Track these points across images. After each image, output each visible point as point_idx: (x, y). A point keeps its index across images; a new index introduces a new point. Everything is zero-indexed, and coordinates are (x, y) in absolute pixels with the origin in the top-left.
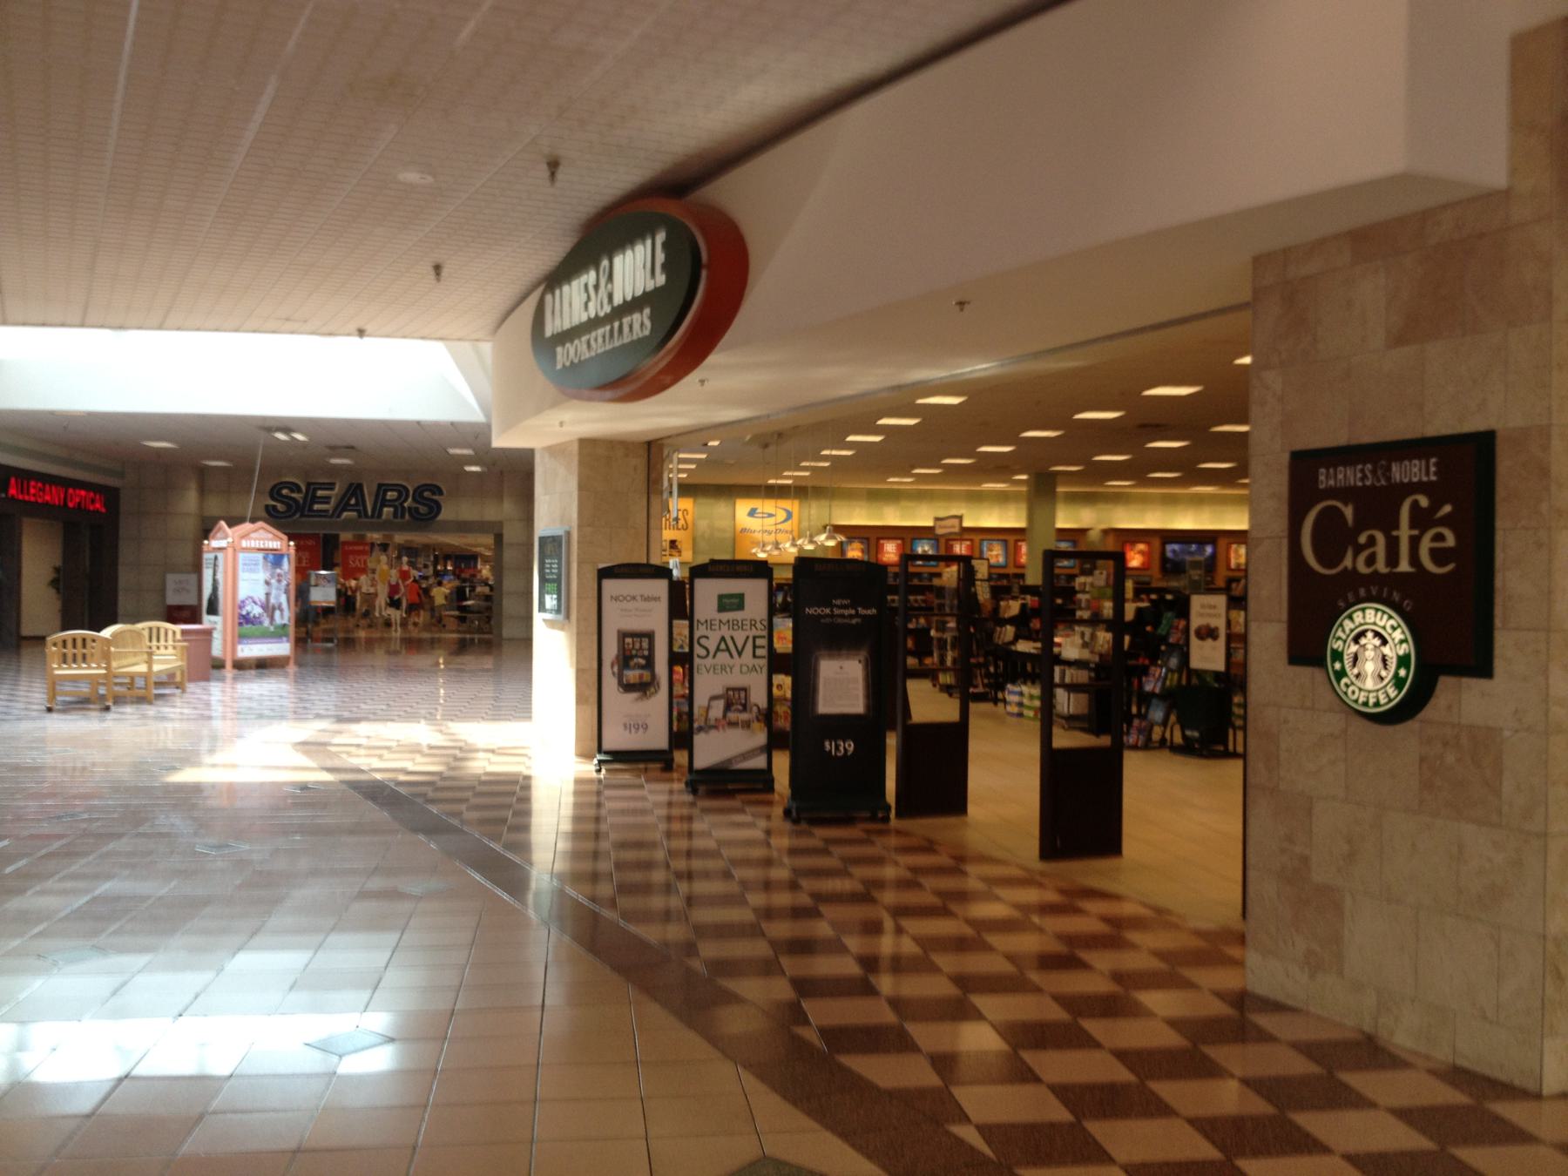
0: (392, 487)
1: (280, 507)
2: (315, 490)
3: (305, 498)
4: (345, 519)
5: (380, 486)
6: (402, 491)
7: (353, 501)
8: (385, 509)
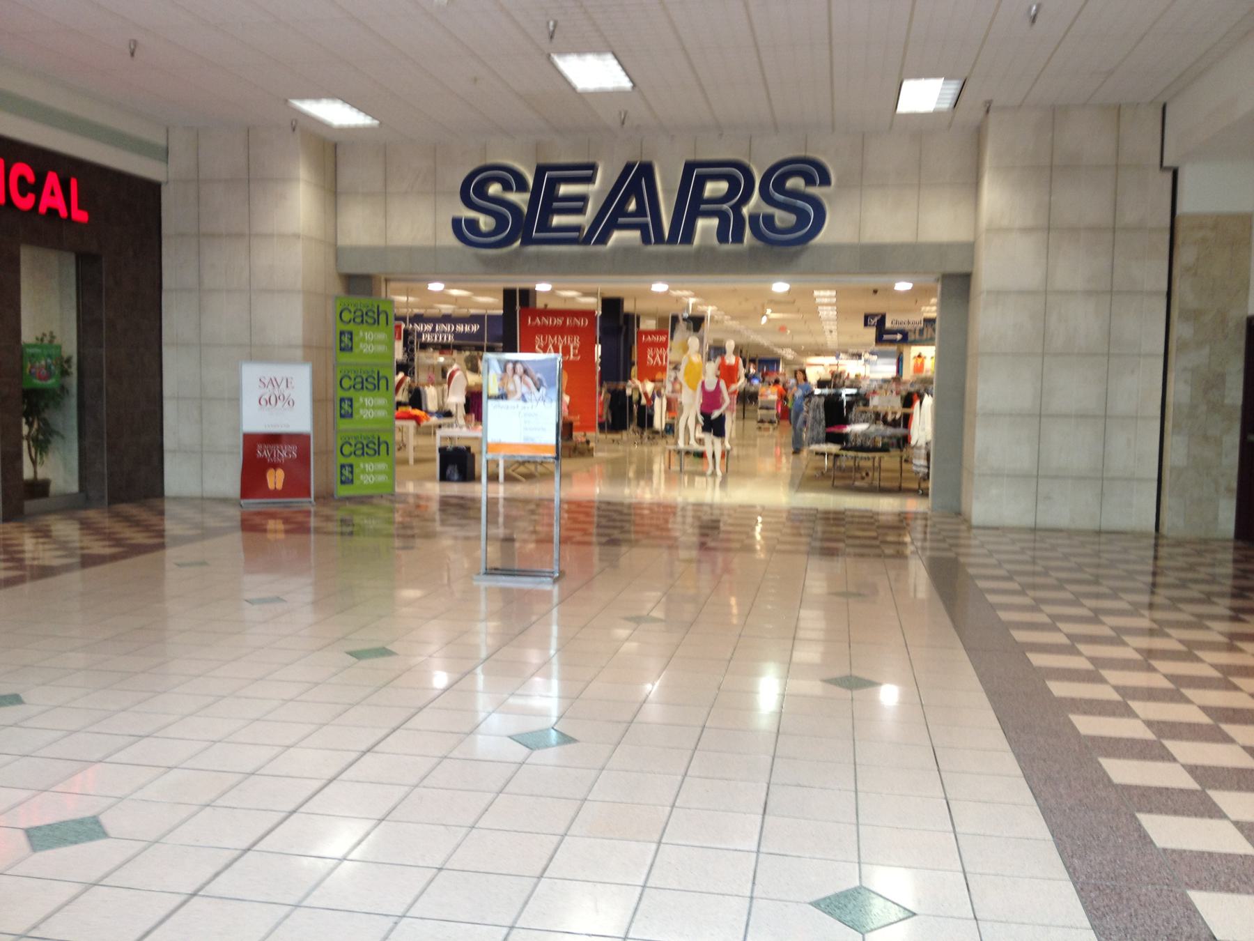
0: (717, 168)
1: (485, 222)
2: (554, 183)
3: (533, 203)
4: (615, 250)
5: (689, 167)
6: (737, 177)
7: (632, 206)
8: (701, 223)
